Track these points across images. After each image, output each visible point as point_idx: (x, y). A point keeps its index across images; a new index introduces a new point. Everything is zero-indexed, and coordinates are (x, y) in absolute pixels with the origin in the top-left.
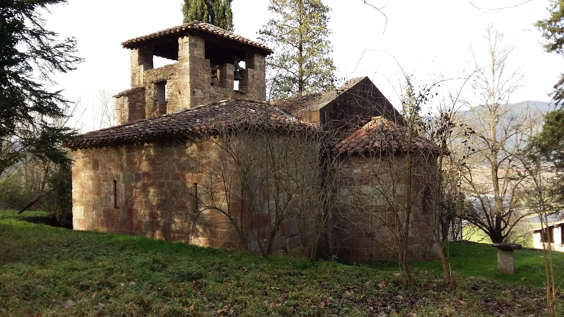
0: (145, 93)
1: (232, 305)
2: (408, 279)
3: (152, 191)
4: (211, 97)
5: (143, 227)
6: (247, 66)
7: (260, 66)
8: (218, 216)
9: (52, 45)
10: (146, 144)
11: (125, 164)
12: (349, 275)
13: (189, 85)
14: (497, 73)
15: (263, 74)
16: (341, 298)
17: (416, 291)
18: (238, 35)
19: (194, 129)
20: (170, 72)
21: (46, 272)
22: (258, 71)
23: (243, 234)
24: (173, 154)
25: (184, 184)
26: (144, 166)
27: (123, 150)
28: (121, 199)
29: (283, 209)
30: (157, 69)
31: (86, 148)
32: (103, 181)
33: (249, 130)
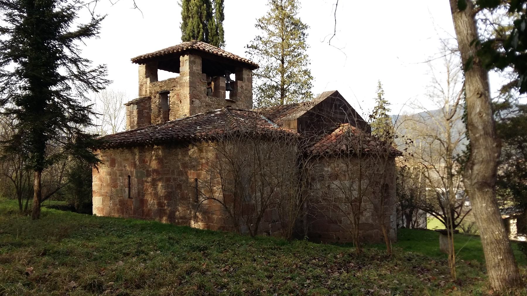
0: (151, 102)
1: (232, 265)
2: (359, 252)
3: (160, 184)
4: (206, 106)
5: (152, 214)
6: (237, 78)
7: (248, 78)
8: (214, 205)
9: (87, 70)
10: (155, 147)
11: (137, 163)
12: (316, 250)
13: (188, 95)
14: (452, 84)
15: (250, 85)
16: (309, 264)
17: (365, 260)
18: (230, 52)
19: (196, 135)
20: (173, 85)
21: (96, 244)
22: (247, 82)
23: (235, 219)
24: (178, 155)
25: (187, 178)
26: (154, 165)
27: (136, 151)
28: (134, 191)
29: (266, 200)
30: (162, 82)
31: (105, 149)
32: (119, 176)
33: (241, 138)
